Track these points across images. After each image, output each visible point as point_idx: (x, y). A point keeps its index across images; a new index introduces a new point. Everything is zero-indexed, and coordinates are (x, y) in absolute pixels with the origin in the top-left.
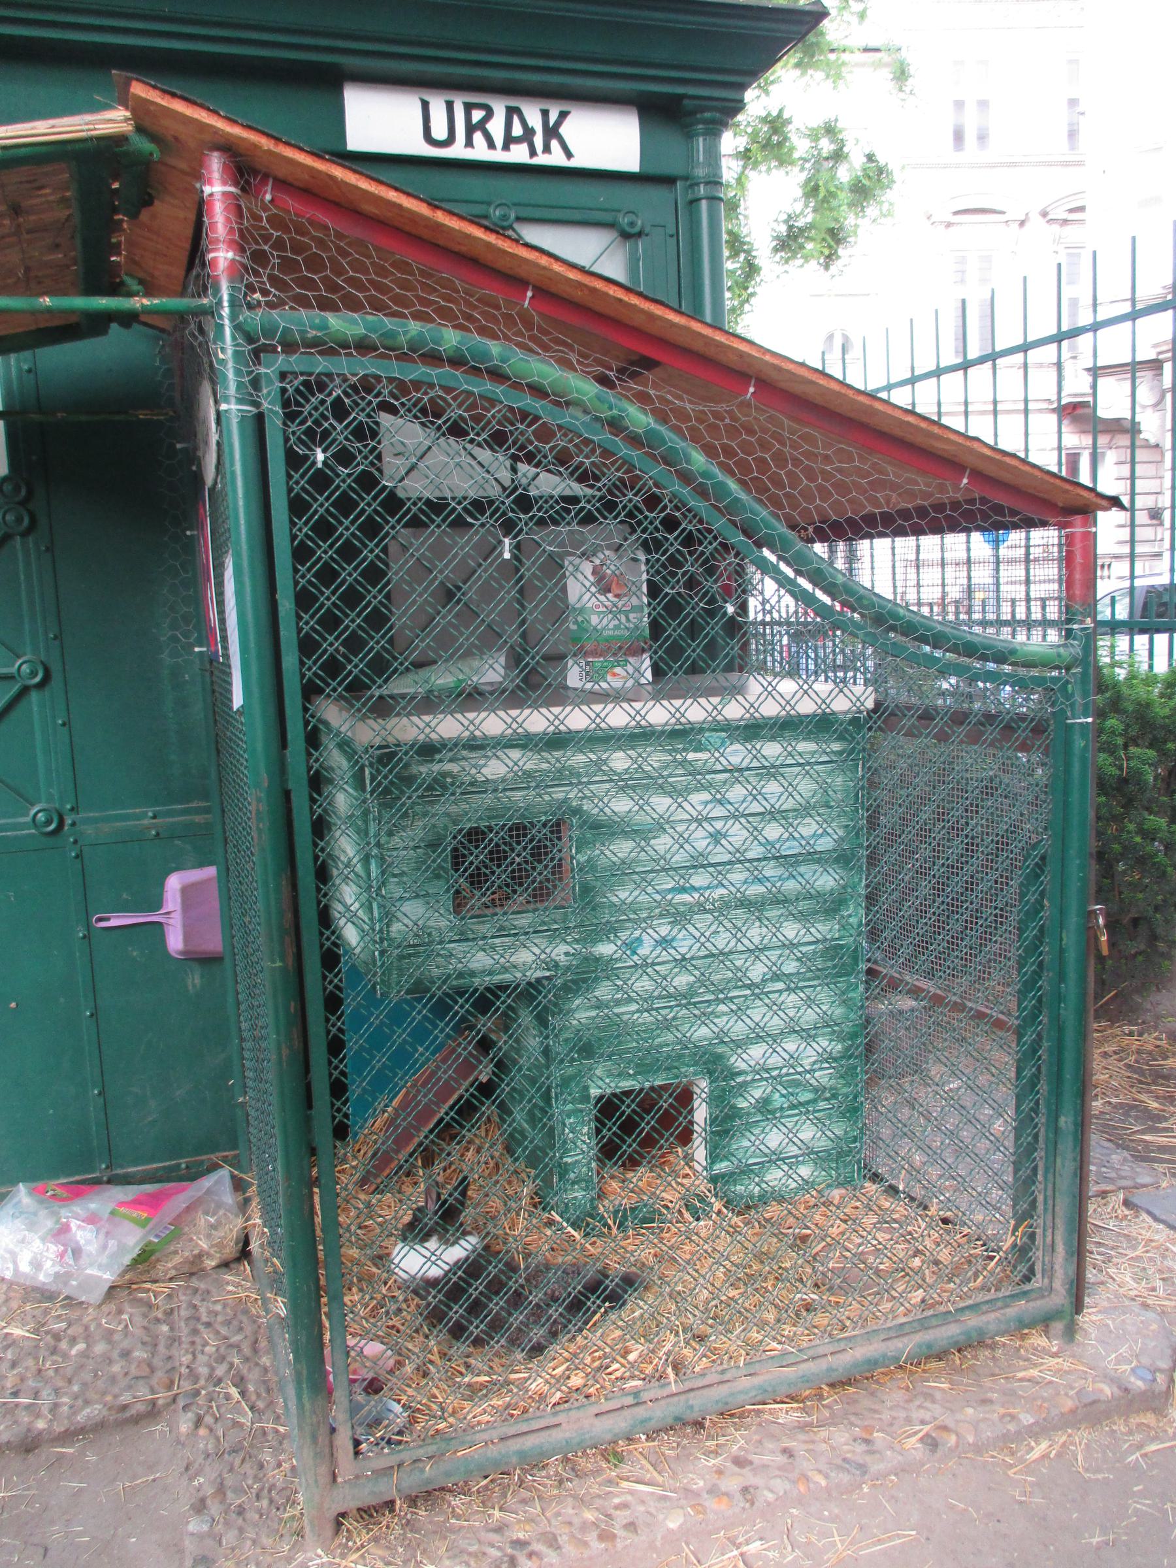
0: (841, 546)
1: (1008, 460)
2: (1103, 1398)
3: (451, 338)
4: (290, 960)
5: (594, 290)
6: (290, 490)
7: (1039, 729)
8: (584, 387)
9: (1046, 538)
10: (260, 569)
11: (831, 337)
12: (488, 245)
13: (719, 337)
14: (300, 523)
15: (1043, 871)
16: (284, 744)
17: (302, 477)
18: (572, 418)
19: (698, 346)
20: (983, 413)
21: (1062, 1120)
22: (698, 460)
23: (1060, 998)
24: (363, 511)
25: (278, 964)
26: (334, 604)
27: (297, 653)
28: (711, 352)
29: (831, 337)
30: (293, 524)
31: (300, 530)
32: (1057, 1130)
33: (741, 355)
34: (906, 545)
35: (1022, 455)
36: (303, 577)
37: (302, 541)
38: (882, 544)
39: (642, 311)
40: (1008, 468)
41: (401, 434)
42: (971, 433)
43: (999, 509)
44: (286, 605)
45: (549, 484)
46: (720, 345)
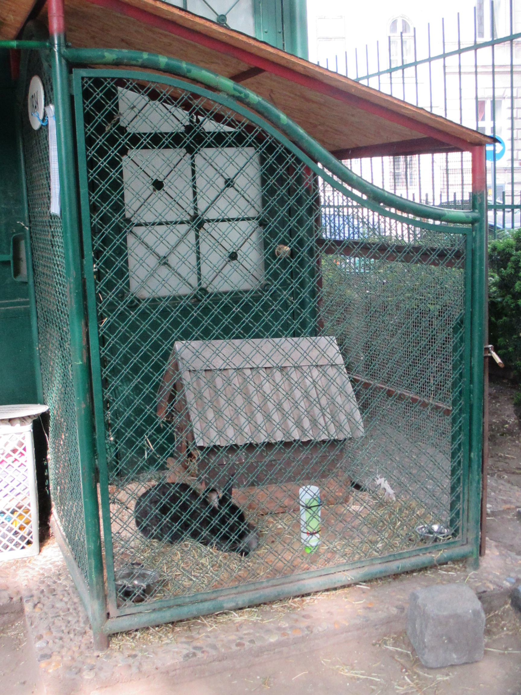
0: (402, 158)
1: (438, 119)
2: (489, 590)
3: (163, 60)
4: (85, 360)
5: (232, 37)
6: (86, 133)
7: (458, 255)
8: (228, 84)
9: (468, 155)
10: (72, 173)
11: (394, 23)
12: (181, 17)
13: (293, 59)
14: (90, 149)
15: (461, 327)
16: (82, 256)
17: (92, 127)
18: (221, 97)
19: (283, 62)
20: (486, 73)
21: (472, 454)
22: (284, 118)
23: (471, 392)
24: (120, 143)
25: (80, 363)
26: (106, 188)
27: (89, 212)
28: (290, 66)
29: (394, 23)
30: (87, 150)
31: (90, 153)
32: (470, 459)
33: (304, 67)
34: (440, 157)
35: (444, 116)
36: (92, 175)
37: (91, 158)
38: (426, 158)
39: (255, 47)
40: (438, 122)
41: (127, 97)
42: (419, 106)
43: (443, 144)
44: (84, 189)
45: (210, 126)
46: (294, 63)
